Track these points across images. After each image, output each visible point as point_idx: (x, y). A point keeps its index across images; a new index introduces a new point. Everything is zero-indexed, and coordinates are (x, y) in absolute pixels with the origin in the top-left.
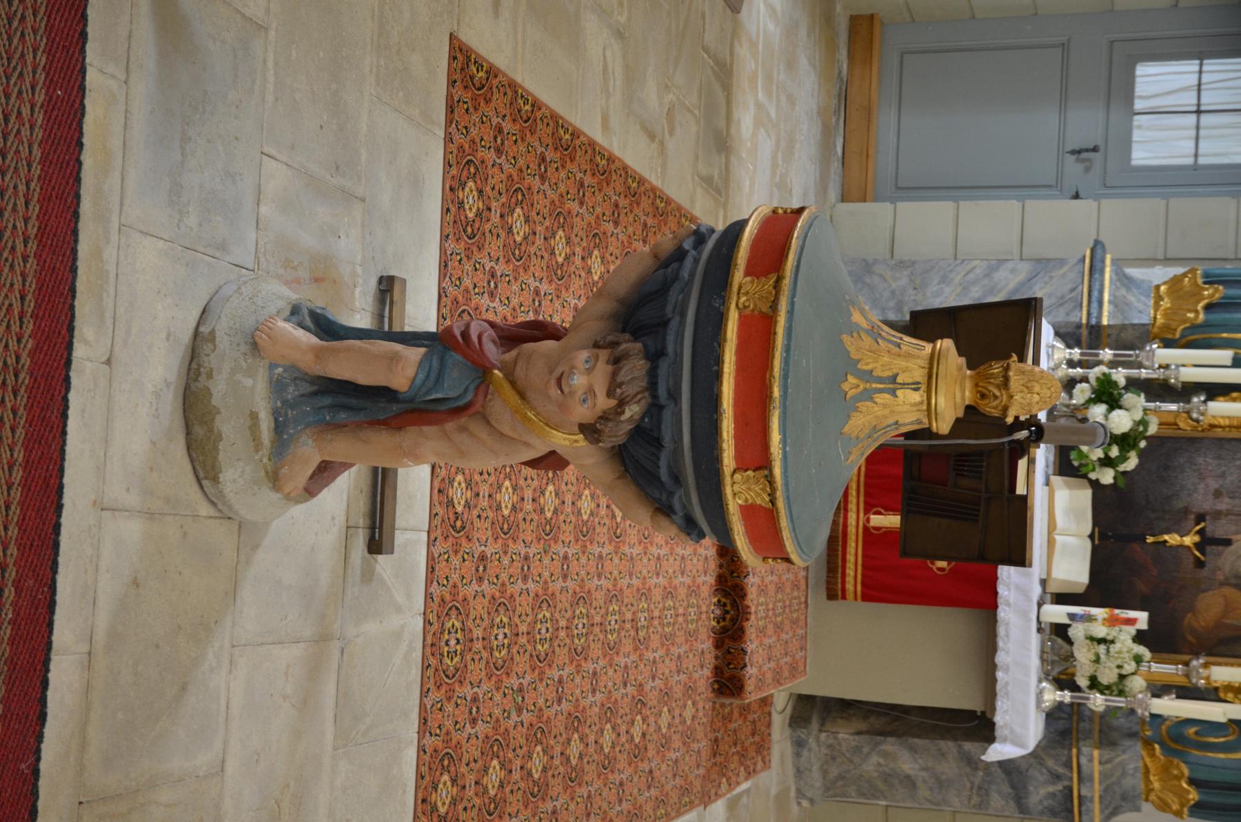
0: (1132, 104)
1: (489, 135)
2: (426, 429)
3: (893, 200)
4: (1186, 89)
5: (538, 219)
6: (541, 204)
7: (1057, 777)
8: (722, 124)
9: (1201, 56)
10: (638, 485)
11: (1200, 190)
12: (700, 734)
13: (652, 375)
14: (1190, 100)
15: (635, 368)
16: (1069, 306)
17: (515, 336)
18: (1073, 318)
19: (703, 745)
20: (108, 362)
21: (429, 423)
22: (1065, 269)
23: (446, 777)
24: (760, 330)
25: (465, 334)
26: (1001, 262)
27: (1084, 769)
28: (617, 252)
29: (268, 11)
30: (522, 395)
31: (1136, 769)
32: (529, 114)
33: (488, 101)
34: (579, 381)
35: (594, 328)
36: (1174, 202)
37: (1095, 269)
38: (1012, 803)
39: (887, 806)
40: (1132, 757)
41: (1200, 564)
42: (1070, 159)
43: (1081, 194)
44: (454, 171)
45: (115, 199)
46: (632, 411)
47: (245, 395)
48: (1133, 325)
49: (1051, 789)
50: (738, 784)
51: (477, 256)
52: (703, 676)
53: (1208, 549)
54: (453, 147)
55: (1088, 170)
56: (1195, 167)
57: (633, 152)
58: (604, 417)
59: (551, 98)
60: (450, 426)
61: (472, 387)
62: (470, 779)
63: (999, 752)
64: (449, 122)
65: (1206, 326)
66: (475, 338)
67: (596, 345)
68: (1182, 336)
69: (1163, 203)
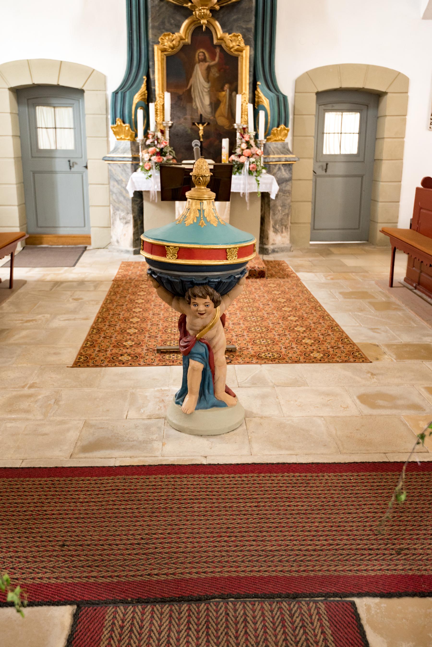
0: (53, 150)
1: (101, 354)
2: (215, 358)
3: (90, 228)
4: (47, 132)
5: (125, 339)
6: (119, 337)
7: (279, 169)
8: (75, 284)
9: (36, 128)
10: (231, 290)
11: (82, 127)
12: (278, 282)
13: (199, 285)
14: (52, 131)
15: (197, 290)
16: (125, 167)
17: (184, 333)
18: (130, 166)
19: (281, 281)
20: (206, 457)
21: (213, 357)
22: (112, 169)
23: (312, 355)
24: (183, 252)
25: (185, 347)
26: (110, 191)
27: (277, 160)
28: (129, 314)
29: (80, 420)
30: (204, 327)
31: (275, 144)
32: (90, 343)
33: (91, 355)
34: (202, 308)
35: (182, 305)
36: (88, 134)
37: (112, 160)
38: (288, 183)
39: (291, 223)
40: (272, 145)
41: (209, 124)
42: (73, 169)
43: (85, 165)
44: (117, 364)
45: (153, 458)
46: (211, 290)
47: (211, 417)
48: (131, 147)
49: (283, 170)
50: (292, 271)
51: (143, 355)
52: (259, 282)
53: (203, 121)
54: (109, 364)
55: (76, 164)
56: (74, 128)
57: (94, 311)
58: (213, 300)
59: (83, 336)
60: (214, 351)
61: (202, 344)
62: (311, 348)
63: (273, 196)
64: (101, 366)
65: (130, 123)
66: (186, 344)
67: (189, 303)
68: (134, 131)
69: (88, 138)
